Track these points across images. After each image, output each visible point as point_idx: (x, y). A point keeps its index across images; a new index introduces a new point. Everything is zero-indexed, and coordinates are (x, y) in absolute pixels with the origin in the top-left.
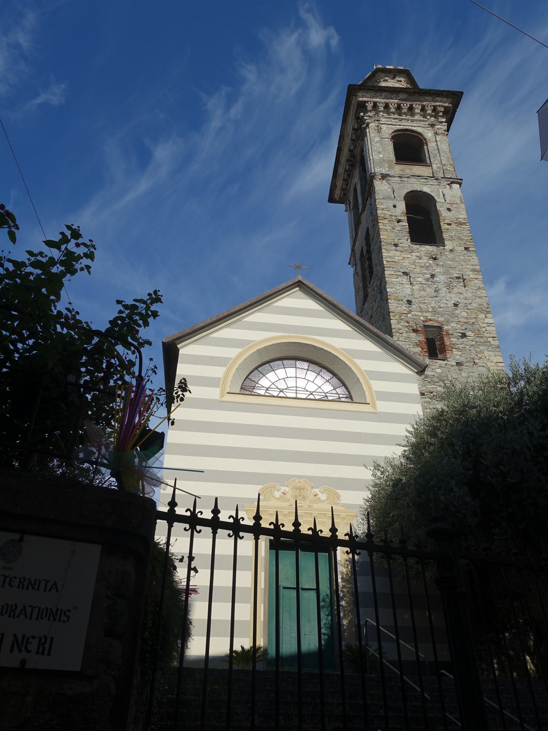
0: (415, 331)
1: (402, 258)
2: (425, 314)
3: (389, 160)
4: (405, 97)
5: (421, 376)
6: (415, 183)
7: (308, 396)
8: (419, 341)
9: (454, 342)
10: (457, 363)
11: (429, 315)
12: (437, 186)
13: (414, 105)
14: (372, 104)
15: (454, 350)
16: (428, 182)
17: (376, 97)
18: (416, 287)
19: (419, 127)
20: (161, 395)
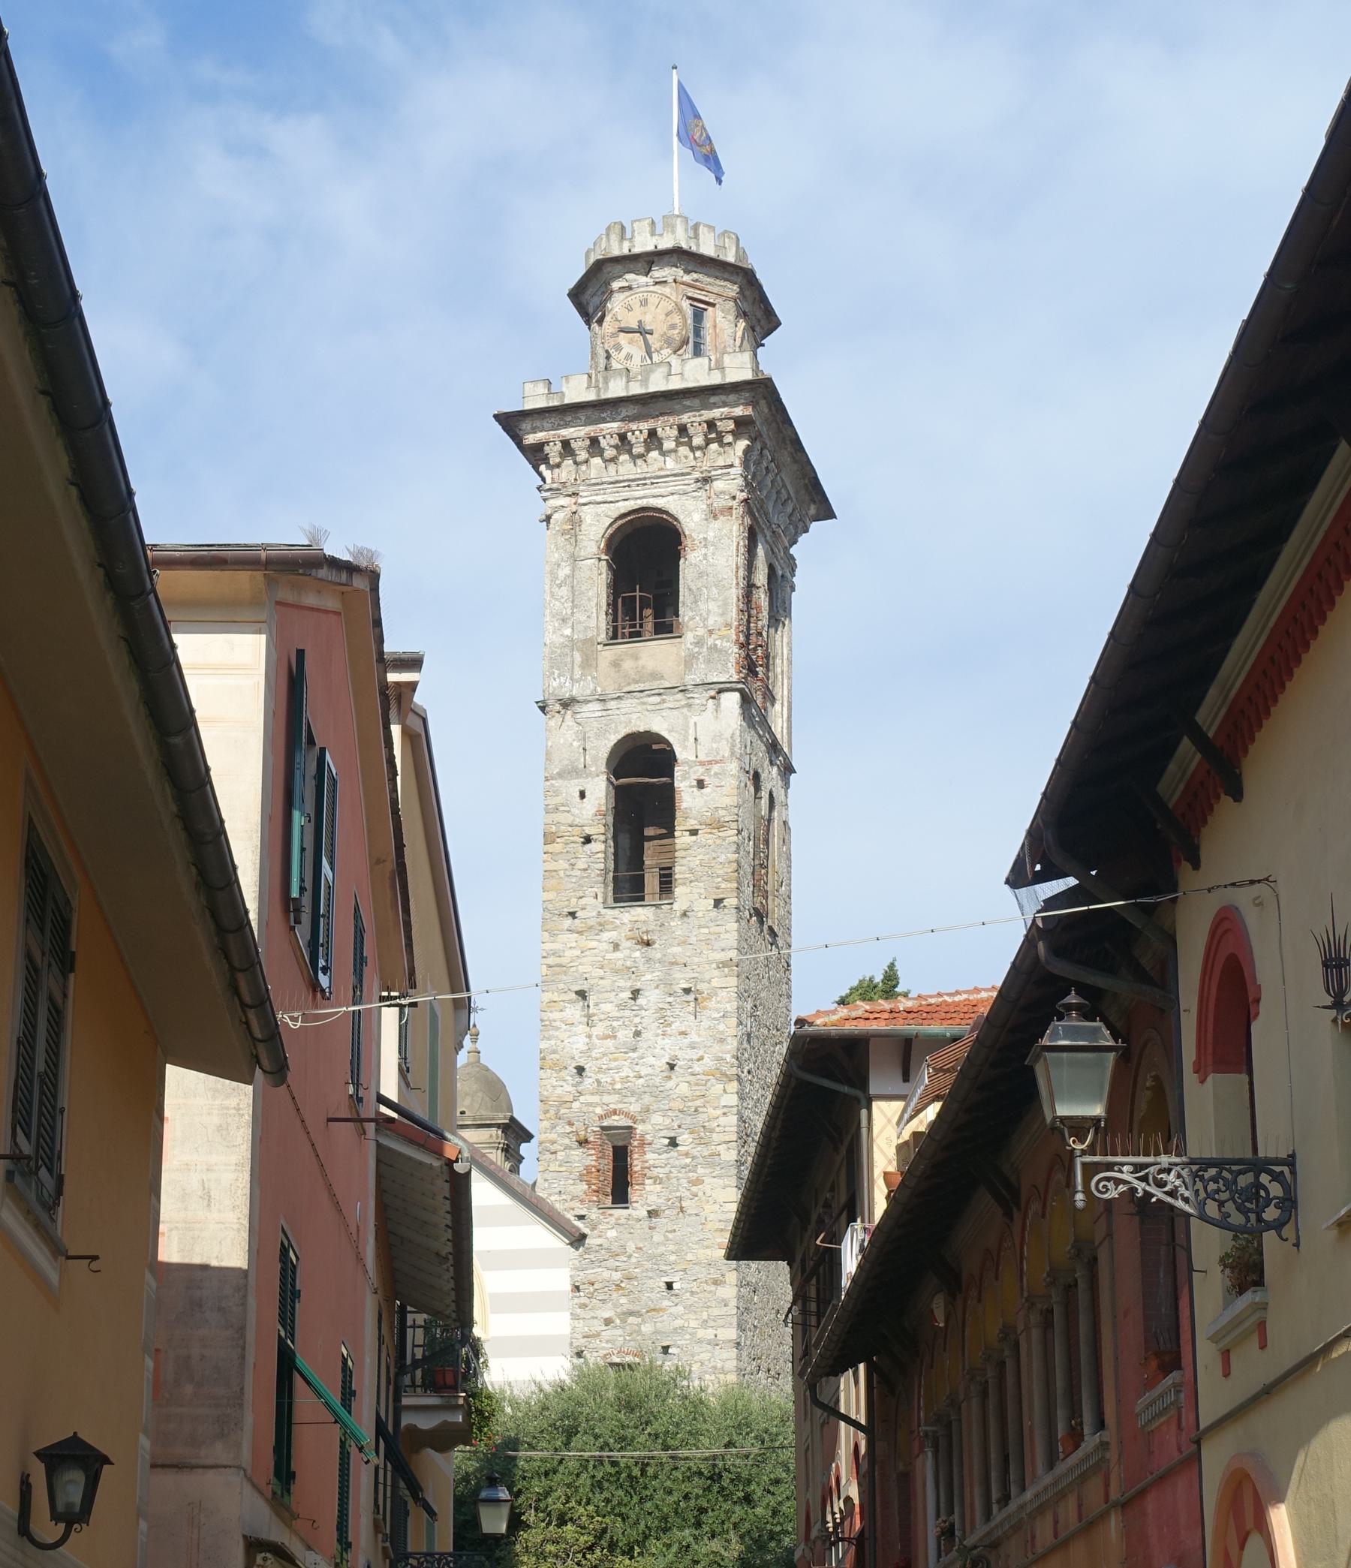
0: (583, 1143)
1: (579, 952)
2: (606, 1099)
3: (585, 641)
4: (635, 411)
5: (577, 1249)
6: (635, 710)
7: (1182, 1247)
8: (587, 1168)
9: (651, 1162)
10: (649, 1212)
11: (612, 1101)
12: (685, 710)
13: (659, 430)
14: (560, 444)
15: (647, 1182)
16: (664, 701)
17: (566, 425)
18: (599, 1030)
19: (672, 494)
20: (1105, 1238)
